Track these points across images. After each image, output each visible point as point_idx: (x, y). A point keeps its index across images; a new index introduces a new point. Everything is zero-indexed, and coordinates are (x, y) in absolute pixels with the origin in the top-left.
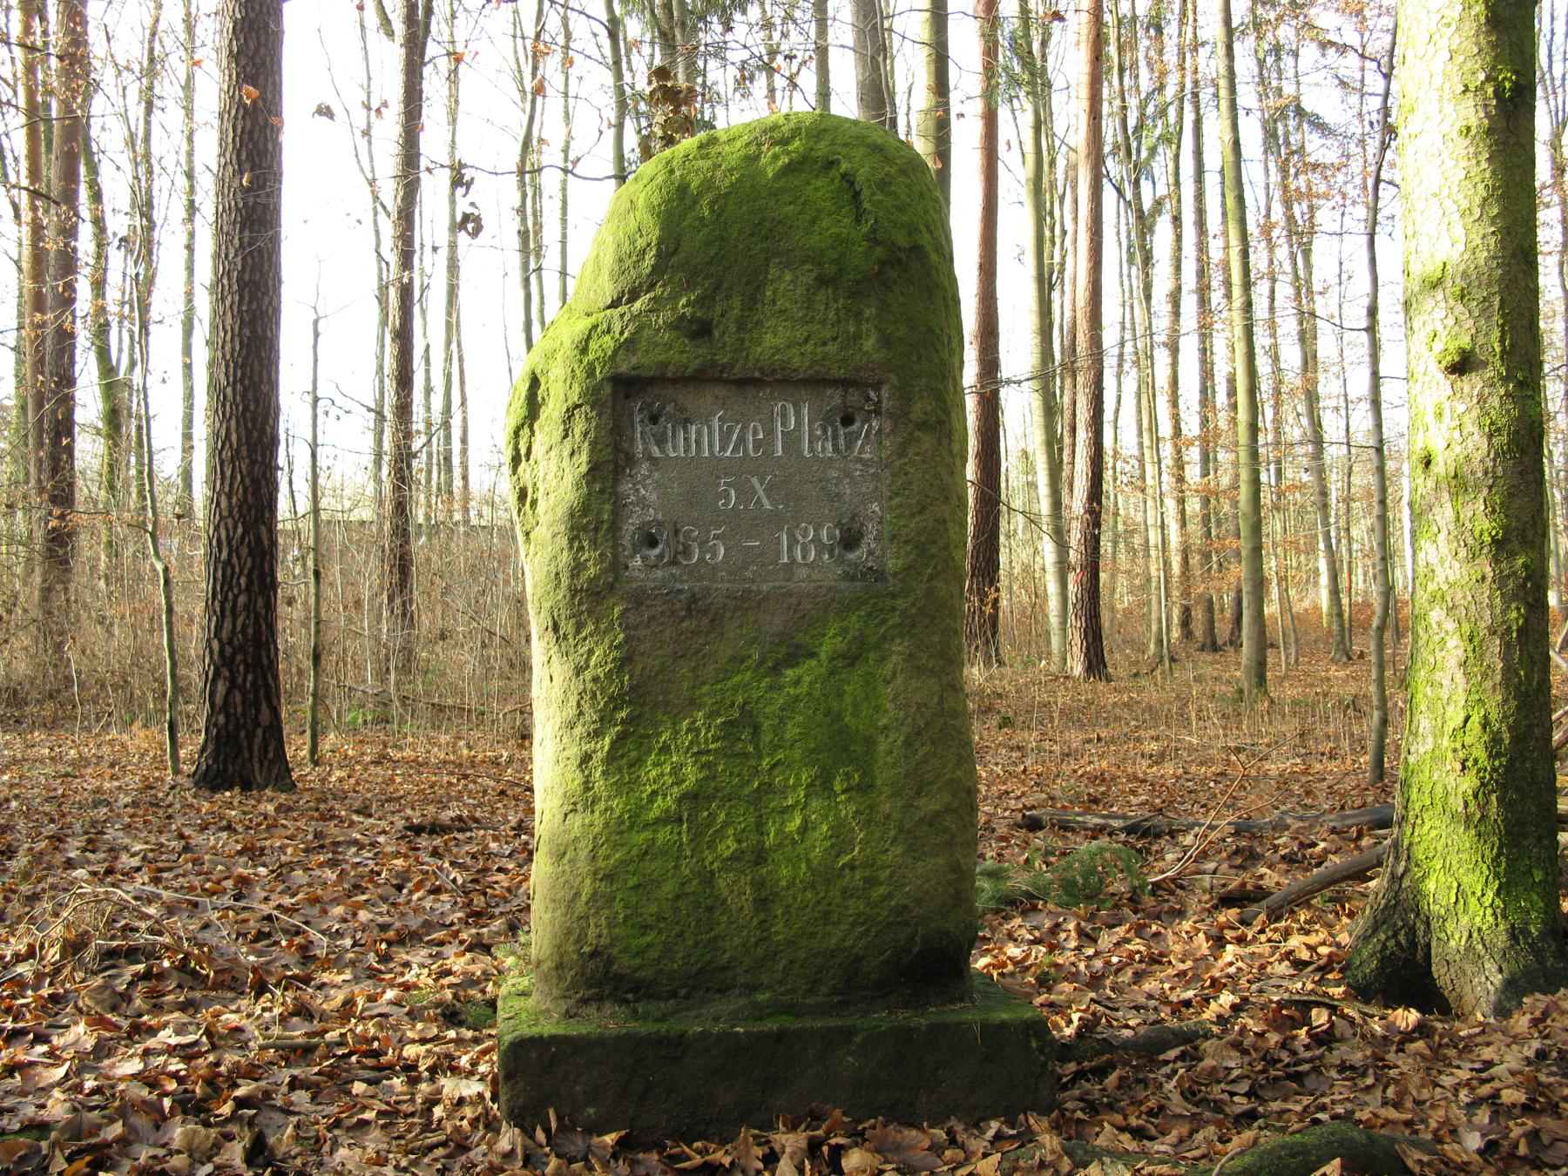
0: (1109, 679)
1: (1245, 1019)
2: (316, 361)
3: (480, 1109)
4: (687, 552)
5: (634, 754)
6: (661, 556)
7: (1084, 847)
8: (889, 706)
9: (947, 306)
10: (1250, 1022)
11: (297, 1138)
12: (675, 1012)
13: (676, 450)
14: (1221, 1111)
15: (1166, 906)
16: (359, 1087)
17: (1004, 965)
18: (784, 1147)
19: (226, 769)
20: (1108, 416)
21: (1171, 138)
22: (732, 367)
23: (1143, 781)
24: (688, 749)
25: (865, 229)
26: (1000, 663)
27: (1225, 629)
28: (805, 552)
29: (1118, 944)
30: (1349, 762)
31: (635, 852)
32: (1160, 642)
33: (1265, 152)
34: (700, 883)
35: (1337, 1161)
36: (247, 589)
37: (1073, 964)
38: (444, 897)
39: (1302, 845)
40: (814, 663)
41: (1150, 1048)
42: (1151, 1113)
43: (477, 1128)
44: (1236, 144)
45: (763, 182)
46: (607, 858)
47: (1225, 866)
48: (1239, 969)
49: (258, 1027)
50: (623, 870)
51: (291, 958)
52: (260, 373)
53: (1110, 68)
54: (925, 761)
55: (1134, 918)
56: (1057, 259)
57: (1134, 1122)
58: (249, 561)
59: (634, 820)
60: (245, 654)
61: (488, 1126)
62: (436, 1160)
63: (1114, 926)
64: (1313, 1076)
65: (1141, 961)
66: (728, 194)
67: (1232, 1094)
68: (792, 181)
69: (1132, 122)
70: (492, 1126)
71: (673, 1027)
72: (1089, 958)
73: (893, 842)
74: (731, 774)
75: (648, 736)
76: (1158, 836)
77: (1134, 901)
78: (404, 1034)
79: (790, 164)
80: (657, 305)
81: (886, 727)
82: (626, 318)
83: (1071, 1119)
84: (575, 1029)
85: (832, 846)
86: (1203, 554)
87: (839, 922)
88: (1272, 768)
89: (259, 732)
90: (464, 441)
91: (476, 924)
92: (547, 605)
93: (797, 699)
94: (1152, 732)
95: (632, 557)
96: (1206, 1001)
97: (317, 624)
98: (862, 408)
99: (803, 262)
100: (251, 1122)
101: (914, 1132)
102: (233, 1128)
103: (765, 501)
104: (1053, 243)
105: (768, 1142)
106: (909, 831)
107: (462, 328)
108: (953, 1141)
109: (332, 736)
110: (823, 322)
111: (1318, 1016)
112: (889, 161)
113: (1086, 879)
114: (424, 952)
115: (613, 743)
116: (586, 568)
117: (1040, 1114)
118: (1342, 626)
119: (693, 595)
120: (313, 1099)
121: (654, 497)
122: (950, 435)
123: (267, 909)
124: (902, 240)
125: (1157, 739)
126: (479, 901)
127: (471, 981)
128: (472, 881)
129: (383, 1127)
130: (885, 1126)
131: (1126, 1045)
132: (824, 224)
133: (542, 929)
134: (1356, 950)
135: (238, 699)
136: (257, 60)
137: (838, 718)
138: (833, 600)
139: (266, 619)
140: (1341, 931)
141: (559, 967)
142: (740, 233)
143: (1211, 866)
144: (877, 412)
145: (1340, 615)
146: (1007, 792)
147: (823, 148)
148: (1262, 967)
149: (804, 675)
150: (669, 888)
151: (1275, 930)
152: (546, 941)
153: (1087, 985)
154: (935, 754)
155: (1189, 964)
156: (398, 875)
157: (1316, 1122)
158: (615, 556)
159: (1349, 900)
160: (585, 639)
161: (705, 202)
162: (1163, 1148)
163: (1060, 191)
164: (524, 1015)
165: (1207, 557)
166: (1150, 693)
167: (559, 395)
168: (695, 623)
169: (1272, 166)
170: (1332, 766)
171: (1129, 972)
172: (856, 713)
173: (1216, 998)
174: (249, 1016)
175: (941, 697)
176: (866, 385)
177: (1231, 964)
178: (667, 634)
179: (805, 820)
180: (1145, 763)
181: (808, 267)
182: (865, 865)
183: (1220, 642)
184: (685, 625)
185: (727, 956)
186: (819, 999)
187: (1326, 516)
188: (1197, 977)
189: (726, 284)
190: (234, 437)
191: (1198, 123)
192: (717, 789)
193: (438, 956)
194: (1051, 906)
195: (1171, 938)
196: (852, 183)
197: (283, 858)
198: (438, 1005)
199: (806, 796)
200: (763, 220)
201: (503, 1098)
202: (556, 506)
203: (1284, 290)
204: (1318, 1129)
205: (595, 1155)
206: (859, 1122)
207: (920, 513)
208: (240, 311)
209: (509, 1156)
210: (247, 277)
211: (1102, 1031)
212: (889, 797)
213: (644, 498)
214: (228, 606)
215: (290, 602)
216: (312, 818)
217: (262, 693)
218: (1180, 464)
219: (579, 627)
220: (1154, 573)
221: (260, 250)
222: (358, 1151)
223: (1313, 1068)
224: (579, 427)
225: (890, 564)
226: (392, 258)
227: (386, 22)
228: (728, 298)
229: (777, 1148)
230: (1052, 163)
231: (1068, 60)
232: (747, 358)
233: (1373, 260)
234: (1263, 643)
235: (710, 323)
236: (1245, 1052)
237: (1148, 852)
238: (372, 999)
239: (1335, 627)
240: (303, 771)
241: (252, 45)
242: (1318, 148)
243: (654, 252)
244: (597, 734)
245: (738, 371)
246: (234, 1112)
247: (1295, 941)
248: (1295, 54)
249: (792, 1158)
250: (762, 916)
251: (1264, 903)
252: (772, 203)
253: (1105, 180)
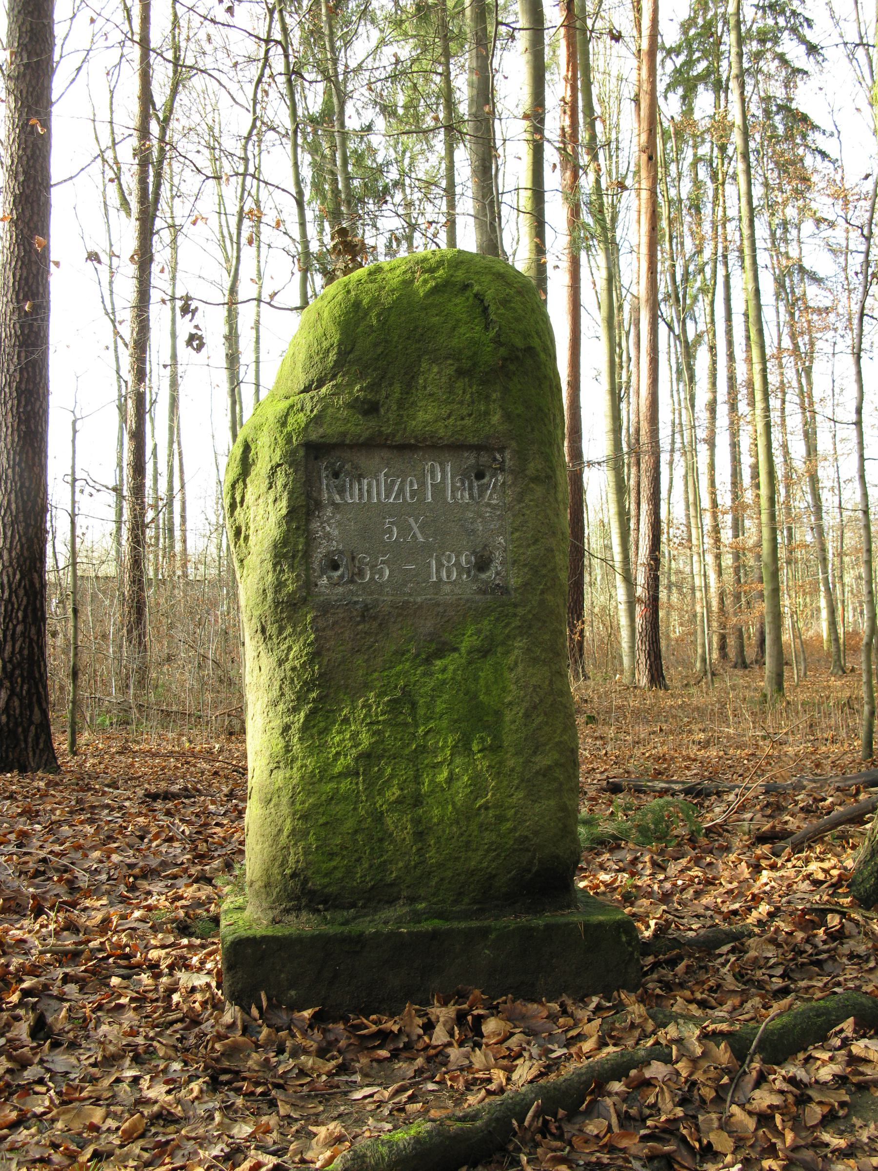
0: (666, 688)
1: (779, 923)
2: (74, 452)
3: (208, 995)
4: (361, 573)
5: (322, 724)
6: (342, 577)
7: (653, 803)
8: (513, 687)
9: (552, 392)
10: (782, 924)
11: (69, 1018)
12: (354, 918)
13: (352, 498)
14: (763, 988)
15: (716, 844)
16: (115, 981)
17: (598, 886)
18: (438, 1017)
19: (7, 757)
20: (664, 494)
21: (708, 290)
22: (394, 436)
23: (695, 760)
24: (363, 720)
25: (492, 334)
26: (586, 677)
27: (752, 651)
28: (448, 573)
29: (682, 871)
30: (846, 745)
31: (324, 798)
32: (704, 660)
33: (777, 299)
34: (373, 821)
35: (851, 1019)
36: (24, 621)
37: (649, 886)
38: (176, 844)
39: (816, 800)
40: (456, 655)
41: (708, 945)
42: (711, 990)
43: (206, 1008)
44: (757, 292)
45: (417, 299)
46: (303, 802)
47: (759, 815)
48: (773, 887)
49: (38, 938)
50: (315, 813)
51: (61, 889)
52: (33, 458)
53: (664, 236)
54: (539, 728)
55: (693, 853)
56: (624, 378)
57: (699, 996)
58: (25, 599)
59: (323, 774)
60: (22, 669)
61: (214, 1007)
62: (176, 1031)
63: (679, 859)
64: (830, 962)
65: (699, 883)
66: (390, 308)
67: (771, 976)
68: (438, 299)
69: (679, 278)
70: (217, 1006)
71: (355, 928)
72: (661, 881)
73: (517, 788)
74: (395, 738)
75: (333, 711)
76: (708, 795)
77: (692, 841)
78: (148, 942)
79: (436, 287)
80: (337, 390)
81: (510, 703)
82: (315, 400)
83: (652, 995)
84: (279, 931)
85: (471, 792)
86: (736, 597)
87: (477, 850)
88: (791, 751)
89: (33, 728)
90: (183, 517)
91: (201, 863)
92: (256, 613)
93: (444, 682)
94: (700, 726)
95: (320, 577)
96: (749, 910)
97: (76, 648)
98: (491, 467)
99: (446, 358)
100: (34, 1007)
101: (535, 1006)
102: (21, 1012)
103: (419, 535)
104: (621, 367)
105: (427, 1014)
106: (529, 781)
107: (182, 431)
108: (564, 1012)
109: (86, 734)
110: (461, 403)
111: (833, 918)
112: (509, 285)
113: (656, 825)
114: (161, 884)
115: (307, 716)
116: (286, 586)
117: (630, 991)
118: (838, 648)
119: (366, 606)
120: (81, 990)
121: (336, 532)
122: (555, 487)
123: (42, 854)
124: (519, 342)
125: (704, 731)
126: (202, 847)
127: (199, 903)
128: (196, 833)
129: (135, 1009)
130: (513, 1001)
131: (690, 942)
132: (462, 331)
133: (254, 861)
134: (859, 871)
135: (17, 703)
136: (32, 225)
137: (475, 697)
138: (470, 608)
139: (37, 643)
140: (847, 858)
141: (267, 885)
142: (400, 336)
143: (748, 816)
144: (502, 469)
145: (837, 640)
146: (594, 769)
147: (460, 275)
148: (789, 886)
149: (448, 665)
150: (349, 825)
151: (798, 859)
152: (257, 867)
153: (660, 900)
154: (547, 723)
155: (735, 884)
156: (141, 829)
157: (835, 993)
158: (307, 576)
159: (852, 837)
160: (285, 638)
161: (373, 314)
162: (721, 1014)
163: (627, 328)
164: (241, 923)
165: (737, 597)
166: (698, 698)
167: (266, 455)
168: (367, 626)
169: (782, 309)
170: (835, 748)
171: (691, 891)
172: (488, 693)
173: (756, 908)
174: (30, 932)
175: (551, 681)
176: (494, 449)
177: (766, 884)
178: (346, 635)
179: (451, 773)
180: (695, 748)
181: (450, 362)
182: (496, 806)
183: (748, 661)
184: (360, 627)
185: (394, 875)
186: (463, 907)
187: (825, 567)
188: (741, 894)
189: (389, 375)
190: (13, 506)
191: (727, 277)
192: (384, 750)
193: (172, 886)
194: (631, 845)
195: (721, 866)
196: (482, 301)
197: (53, 817)
198: (173, 921)
199: (451, 755)
200: (416, 327)
201: (225, 985)
202: (263, 539)
203: (792, 397)
204: (836, 997)
205: (296, 1026)
206: (494, 999)
207: (534, 543)
208: (18, 412)
209: (231, 1027)
210: (23, 386)
211: (672, 933)
212: (513, 755)
213: (329, 533)
214: (9, 633)
215: (54, 634)
216: (74, 790)
217: (34, 699)
218: (716, 529)
219: (281, 630)
220: (698, 609)
221: (36, 361)
222: (116, 1026)
223: (830, 957)
224: (280, 480)
225: (512, 581)
226: (129, 377)
227: (125, 203)
228: (391, 385)
229: (433, 1018)
230: (620, 307)
231: (632, 231)
232: (405, 429)
233: (859, 373)
234: (781, 662)
235: (377, 403)
236: (779, 946)
237: (702, 806)
238: (123, 917)
239: (833, 649)
240: (67, 760)
241: (27, 214)
242: (815, 295)
243: (336, 350)
244: (295, 710)
246: (21, 1000)
247: (814, 866)
248: (798, 227)
249: (444, 1025)
250: (420, 845)
251: (789, 840)
252: (423, 315)
253: (660, 320)
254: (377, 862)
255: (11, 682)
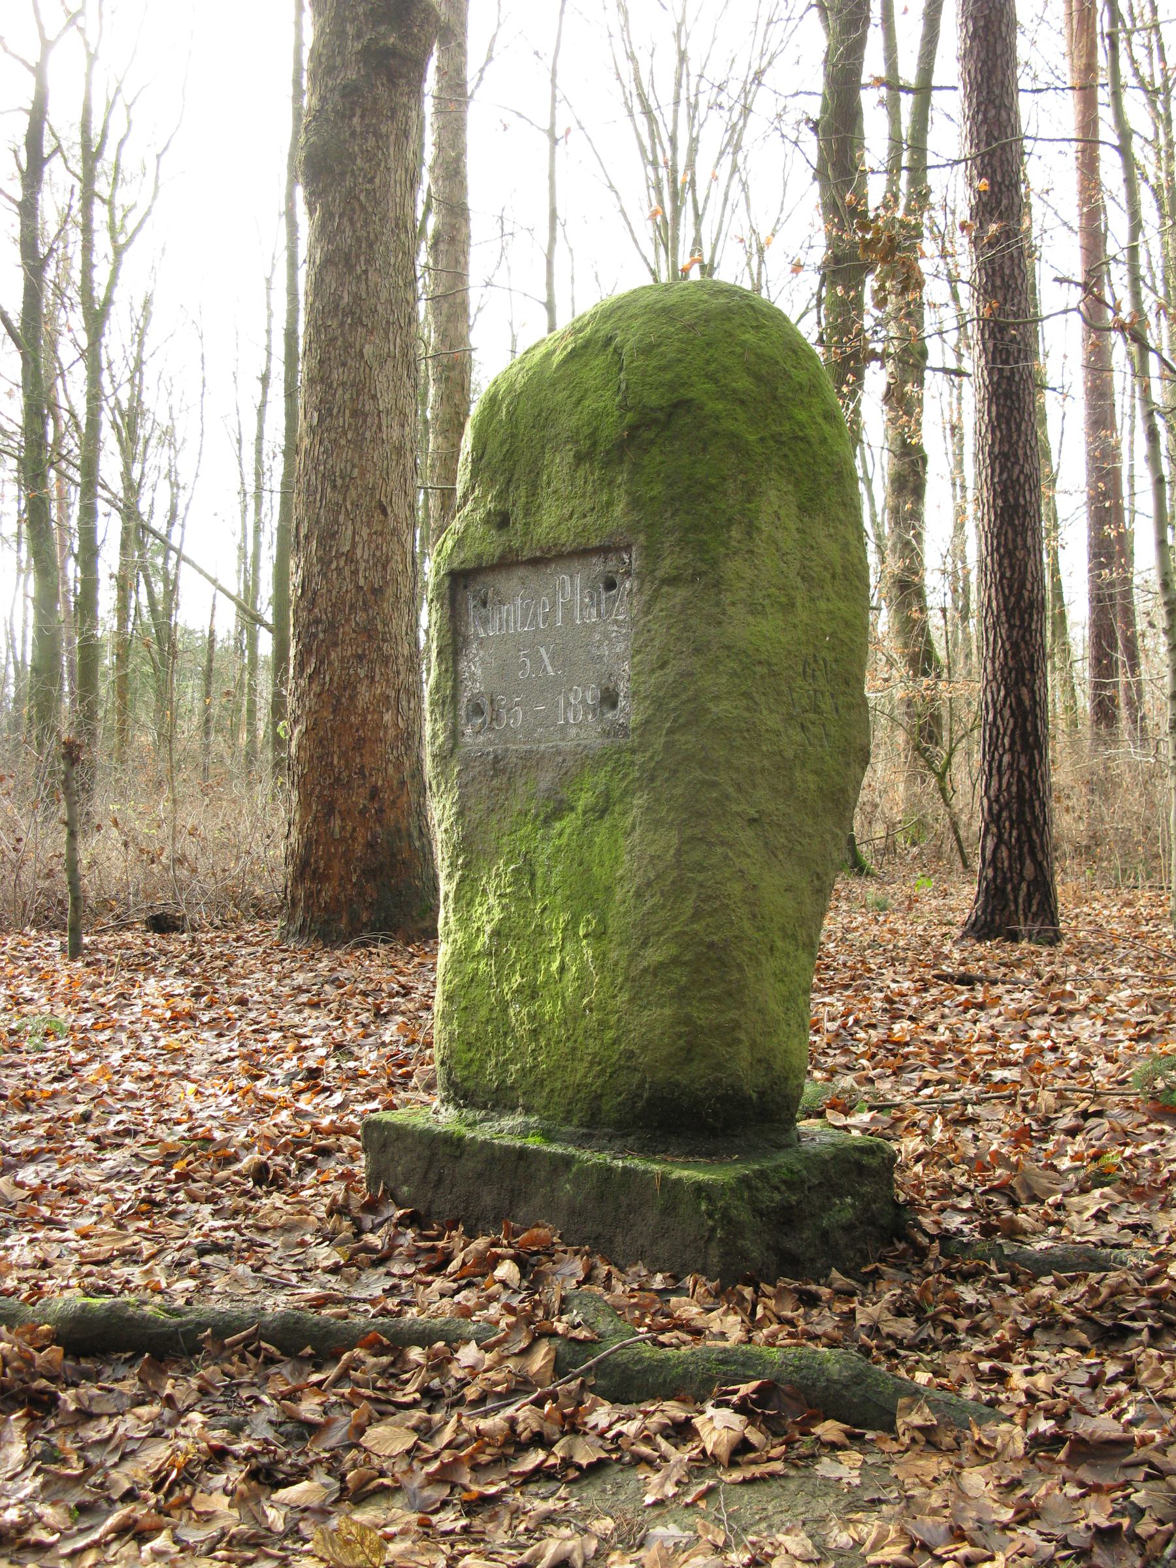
8: (626, 857)
12: (482, 1121)
19: (993, 921)
36: (1011, 749)
52: (1014, 541)
60: (1010, 811)
81: (622, 878)
89: (1024, 886)
99: (566, 443)
103: (549, 668)
106: (633, 981)
135: (1005, 854)
139: (1029, 777)
190: (994, 604)
208: (993, 484)
214: (995, 765)
217: (1026, 849)
245: (526, 554)
254: (501, 1059)
255: (998, 828)
